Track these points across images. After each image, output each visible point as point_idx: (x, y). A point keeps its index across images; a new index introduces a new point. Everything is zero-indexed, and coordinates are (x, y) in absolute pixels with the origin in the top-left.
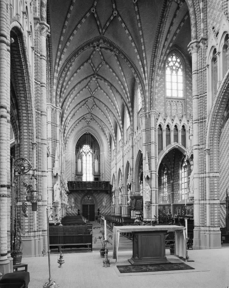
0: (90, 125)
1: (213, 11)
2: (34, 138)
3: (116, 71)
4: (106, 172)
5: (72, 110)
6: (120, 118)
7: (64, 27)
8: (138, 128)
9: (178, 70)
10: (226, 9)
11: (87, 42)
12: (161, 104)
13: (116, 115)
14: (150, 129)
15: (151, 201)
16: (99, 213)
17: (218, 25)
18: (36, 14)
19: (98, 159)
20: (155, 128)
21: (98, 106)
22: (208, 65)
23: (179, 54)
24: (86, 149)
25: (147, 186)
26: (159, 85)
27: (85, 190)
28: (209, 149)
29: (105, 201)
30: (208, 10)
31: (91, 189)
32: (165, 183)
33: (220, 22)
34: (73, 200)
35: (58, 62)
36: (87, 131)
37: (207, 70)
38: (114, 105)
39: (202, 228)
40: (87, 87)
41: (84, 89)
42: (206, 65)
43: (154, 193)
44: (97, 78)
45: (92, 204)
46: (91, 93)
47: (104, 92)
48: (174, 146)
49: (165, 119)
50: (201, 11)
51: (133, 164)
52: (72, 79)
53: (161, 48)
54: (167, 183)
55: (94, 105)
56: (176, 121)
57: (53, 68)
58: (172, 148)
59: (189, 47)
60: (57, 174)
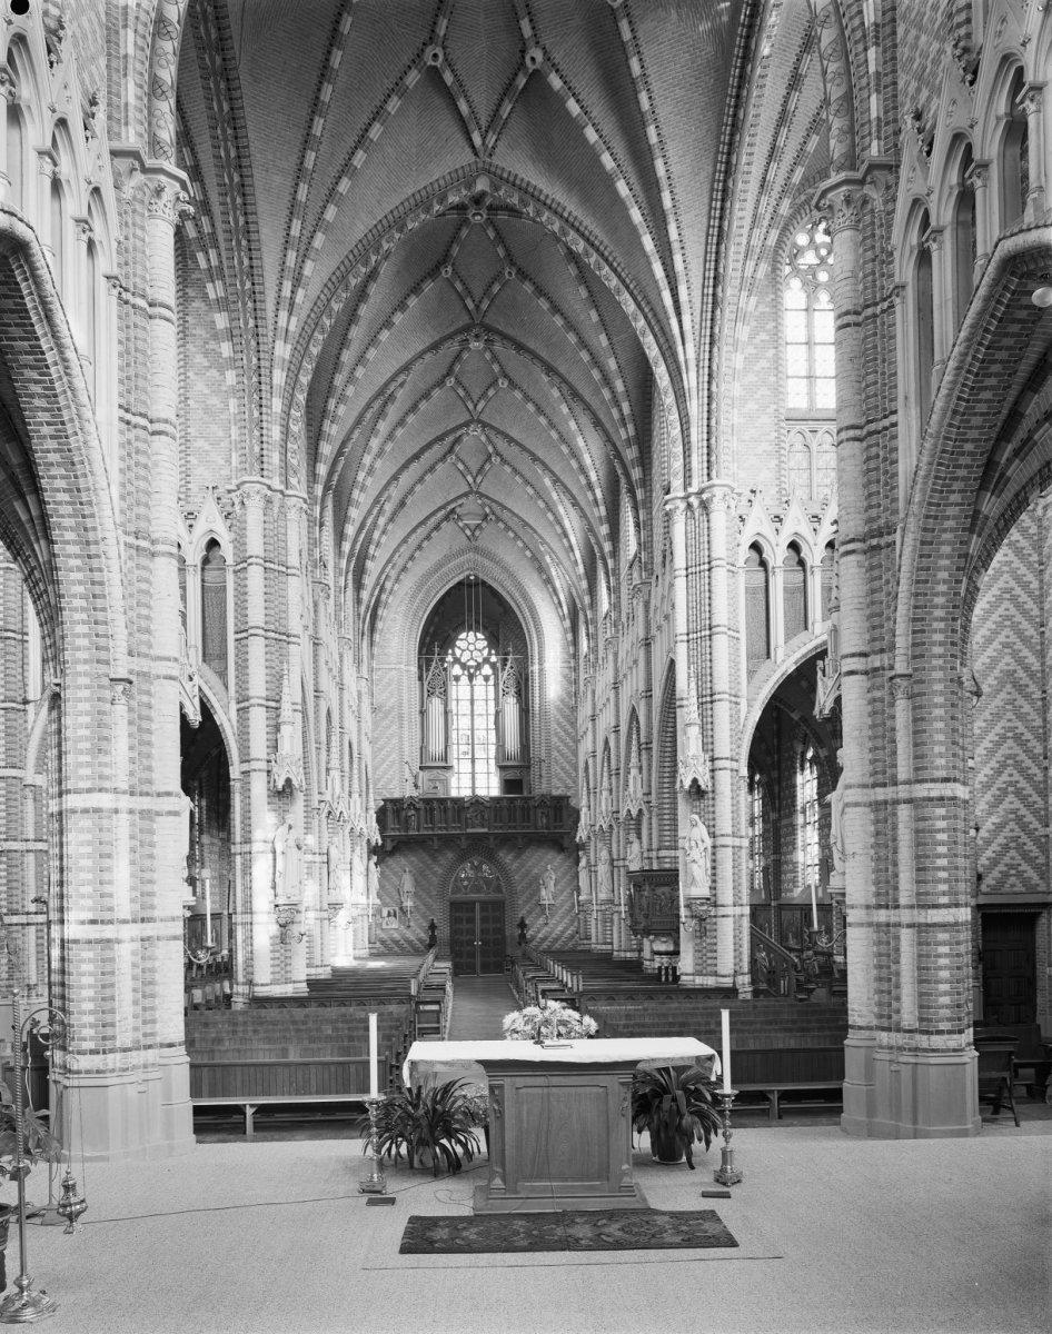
0: (480, 543)
1: (917, 38)
3: (565, 307)
4: (555, 753)
6: (603, 510)
7: (307, 141)
10: (962, 31)
11: (418, 196)
13: (584, 499)
16: (523, 936)
18: (127, 132)
20: (730, 560)
24: (471, 648)
25: (695, 829)
27: (458, 837)
28: (910, 671)
29: (552, 883)
30: (900, 31)
31: (486, 830)
34: (408, 883)
35: (288, 294)
36: (467, 573)
37: (898, 309)
38: (575, 454)
39: (884, 1037)
40: (450, 382)
41: (436, 393)
45: (493, 896)
46: (471, 407)
50: (870, 39)
52: (372, 354)
53: (751, 197)
55: (490, 456)
57: (270, 321)
58: (816, 648)
60: (288, 781)
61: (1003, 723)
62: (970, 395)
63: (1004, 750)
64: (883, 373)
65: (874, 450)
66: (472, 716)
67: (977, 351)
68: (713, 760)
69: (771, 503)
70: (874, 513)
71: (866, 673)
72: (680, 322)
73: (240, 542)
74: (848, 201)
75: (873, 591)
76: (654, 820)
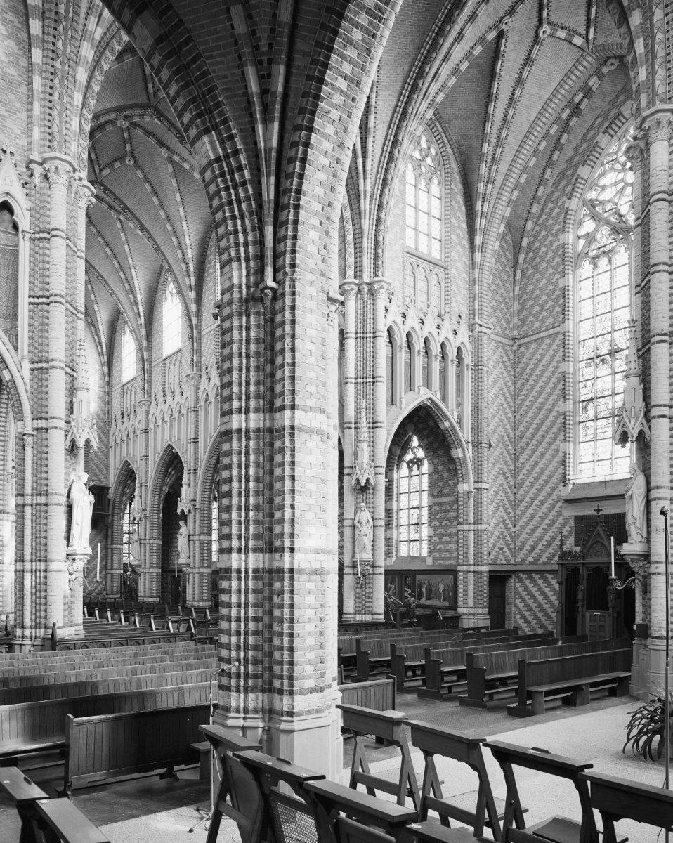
21: (95, 222)
47: (147, 179)
61: (498, 465)
63: (499, 482)
72: (364, 162)
73: (40, 210)
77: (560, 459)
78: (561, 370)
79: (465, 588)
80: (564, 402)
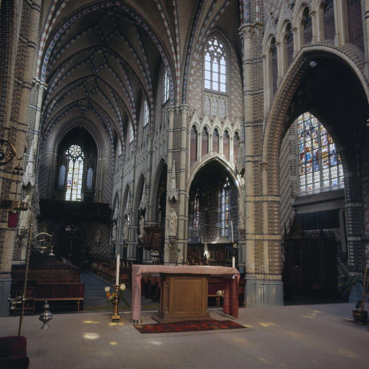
2: (7, 120)
5: (61, 91)
8: (161, 127)
9: (220, 58)
12: (197, 98)
14: (180, 130)
15: (178, 236)
17: (277, 12)
19: (93, 168)
22: (265, 56)
23: (222, 39)
24: (75, 150)
25: (173, 213)
26: (195, 72)
32: (197, 210)
33: (280, 9)
37: (264, 62)
40: (89, 61)
42: (262, 56)
43: (181, 222)
44: (104, 51)
48: (213, 157)
49: (201, 118)
51: (151, 178)
53: (200, 27)
54: (200, 211)
56: (217, 123)
59: (240, 31)
62: (289, 87)
64: (259, 78)
65: (256, 99)
66: (73, 174)
67: (292, 75)
68: (179, 191)
69: (199, 114)
70: (256, 116)
71: (253, 162)
74: (250, 31)
75: (256, 138)
76: (150, 212)
77: (290, 185)
78: (289, 140)
79: (241, 253)
80: (291, 155)
